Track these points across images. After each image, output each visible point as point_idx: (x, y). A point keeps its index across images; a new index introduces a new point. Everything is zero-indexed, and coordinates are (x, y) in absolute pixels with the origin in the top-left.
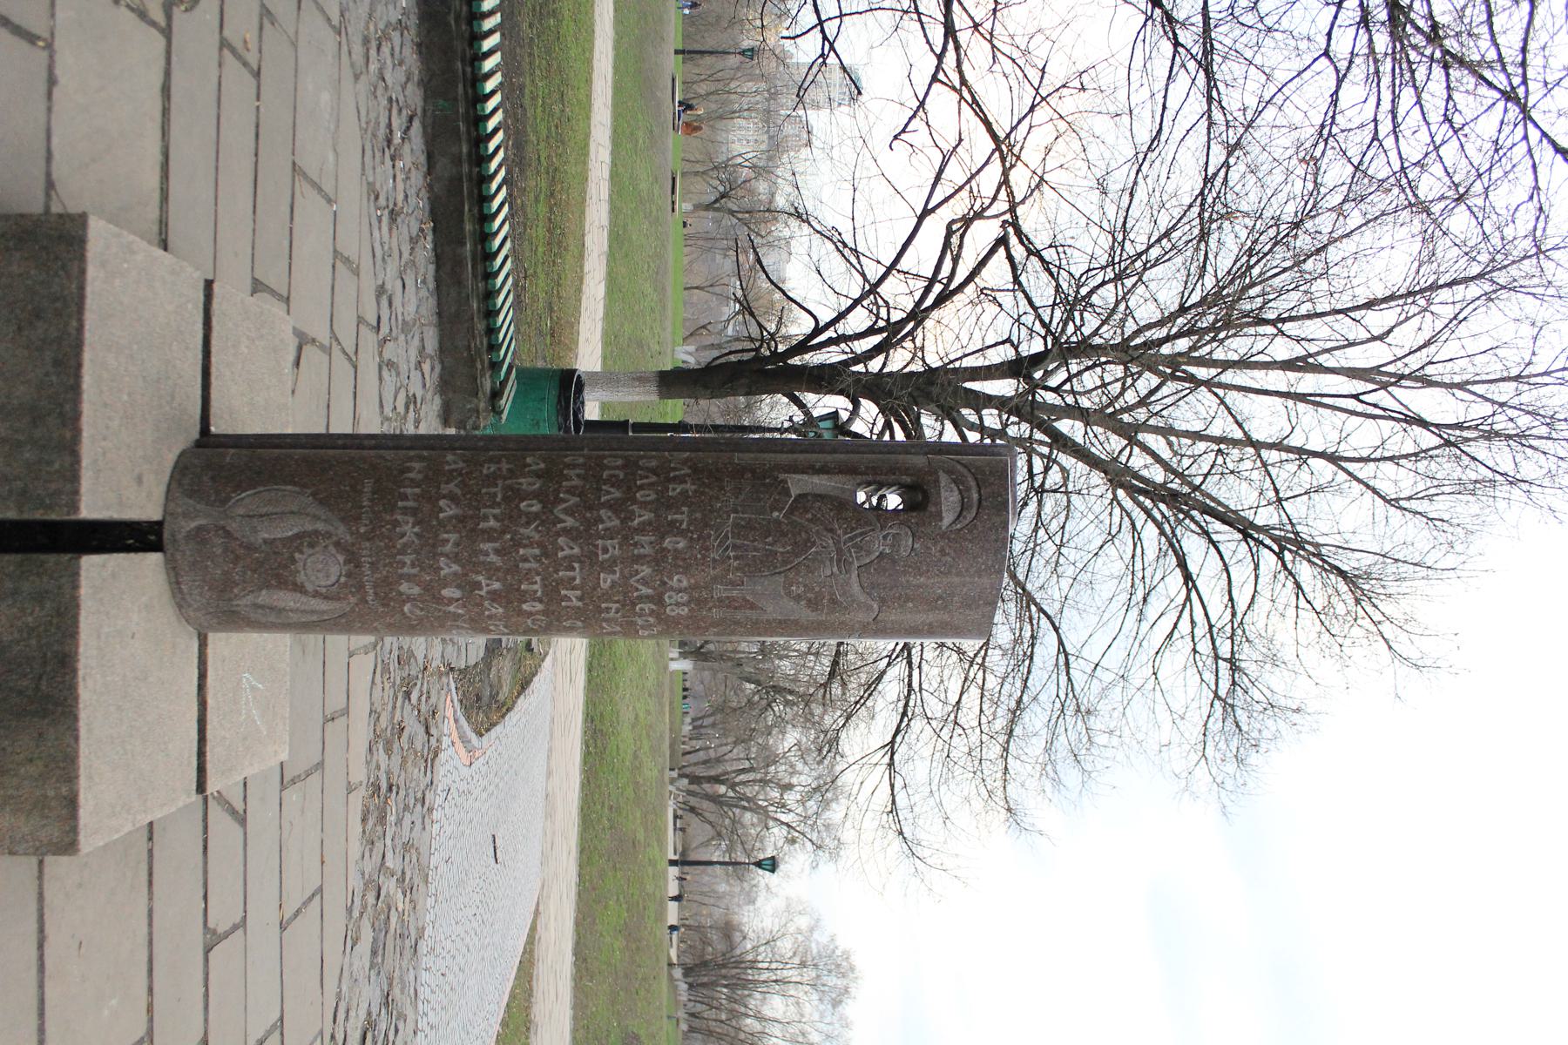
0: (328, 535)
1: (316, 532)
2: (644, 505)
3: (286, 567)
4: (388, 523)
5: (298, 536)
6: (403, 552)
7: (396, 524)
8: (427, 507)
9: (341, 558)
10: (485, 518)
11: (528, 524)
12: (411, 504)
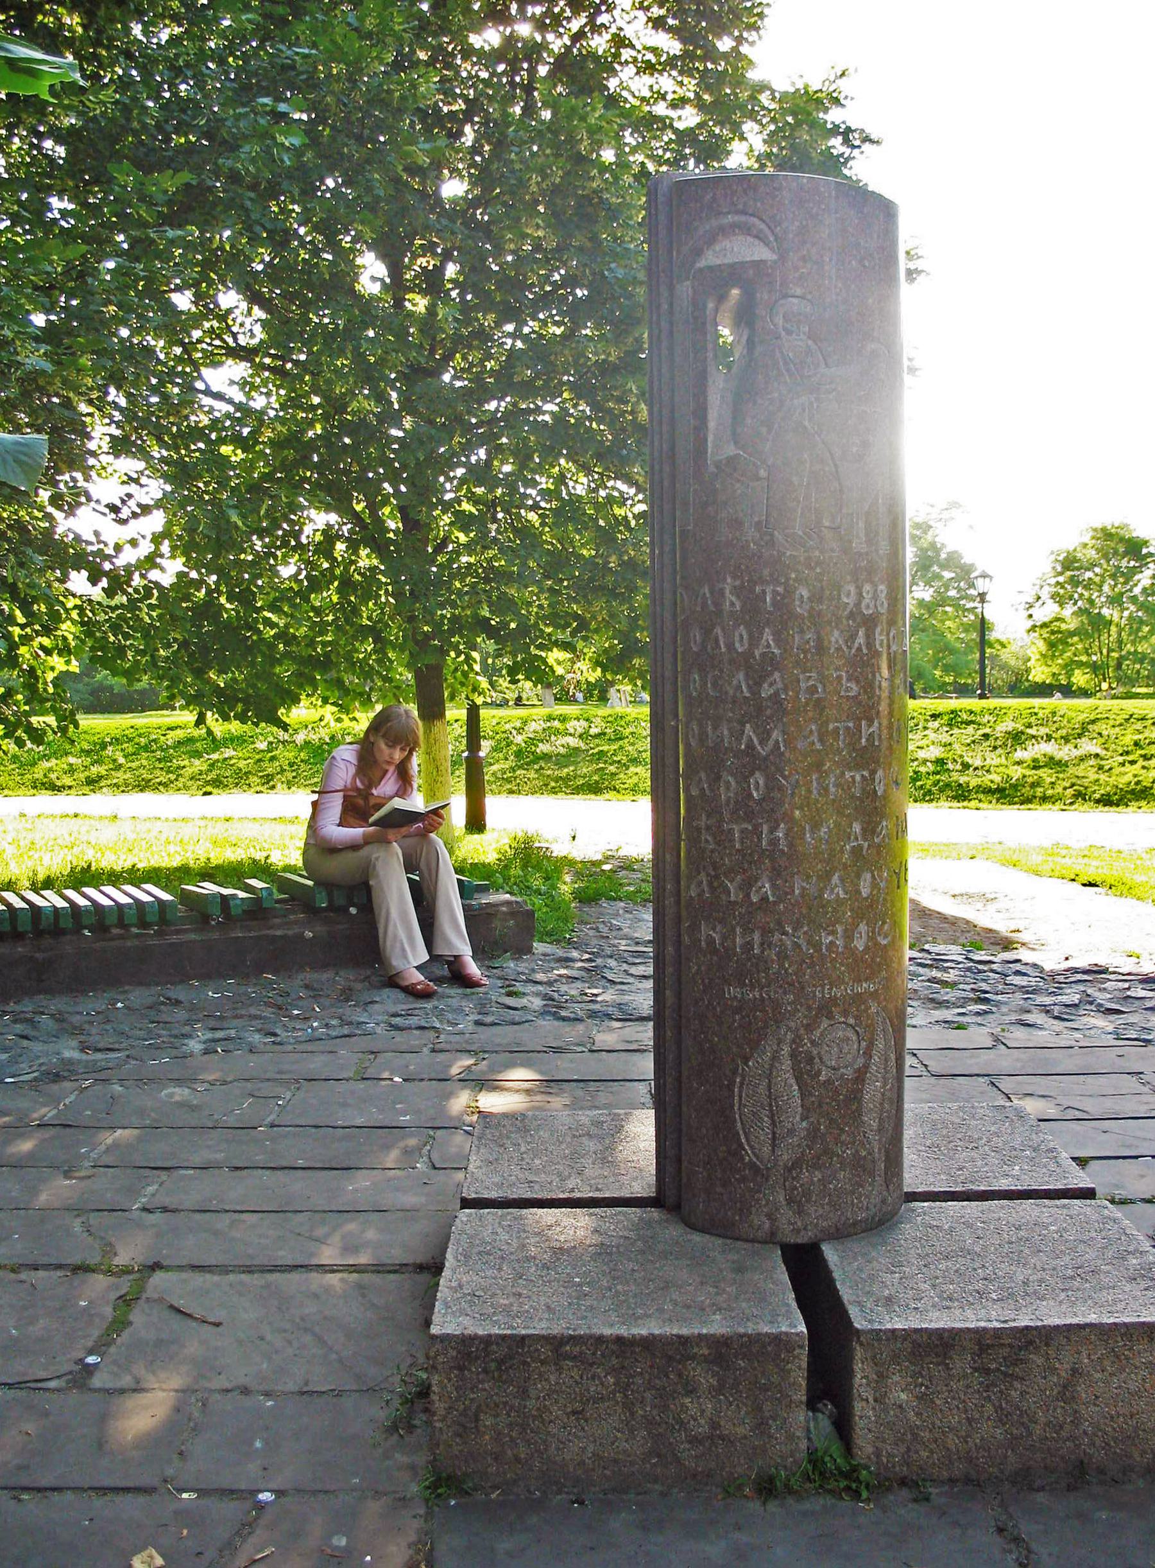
0: (797, 1040)
1: (793, 1055)
2: (754, 640)
3: (837, 1092)
4: (782, 966)
5: (799, 1080)
6: (817, 946)
7: (782, 956)
8: (760, 917)
9: (825, 1023)
10: (774, 842)
11: (781, 789)
12: (757, 936)
